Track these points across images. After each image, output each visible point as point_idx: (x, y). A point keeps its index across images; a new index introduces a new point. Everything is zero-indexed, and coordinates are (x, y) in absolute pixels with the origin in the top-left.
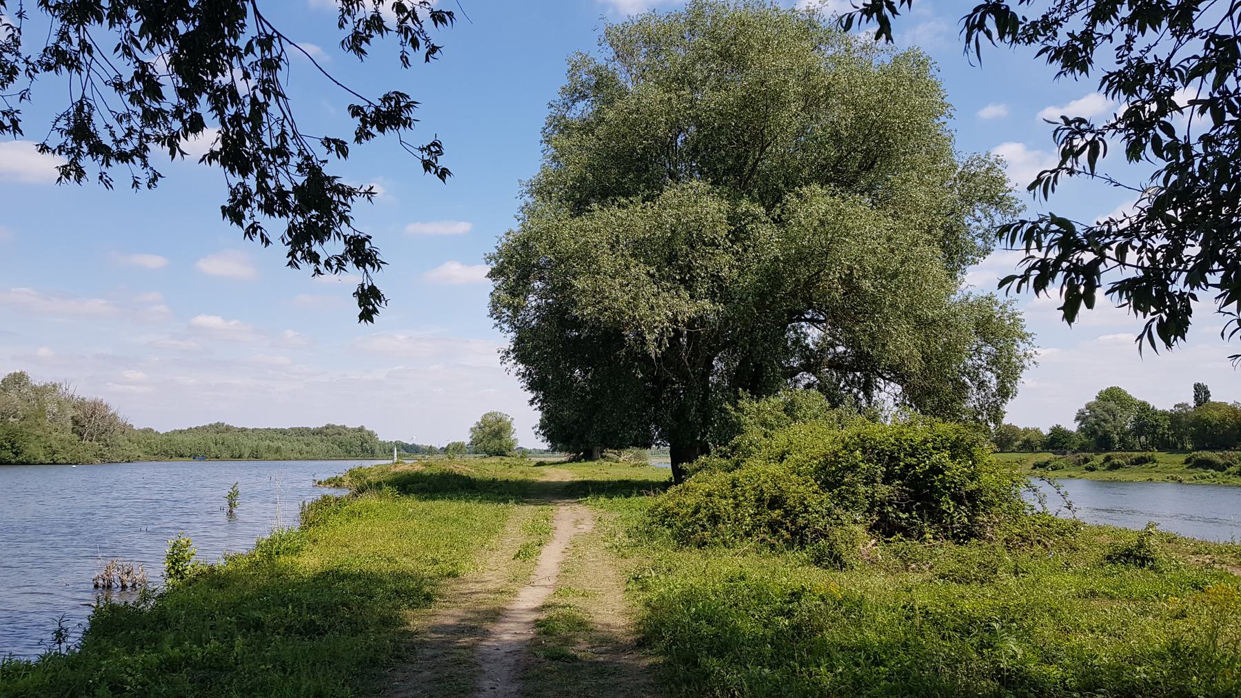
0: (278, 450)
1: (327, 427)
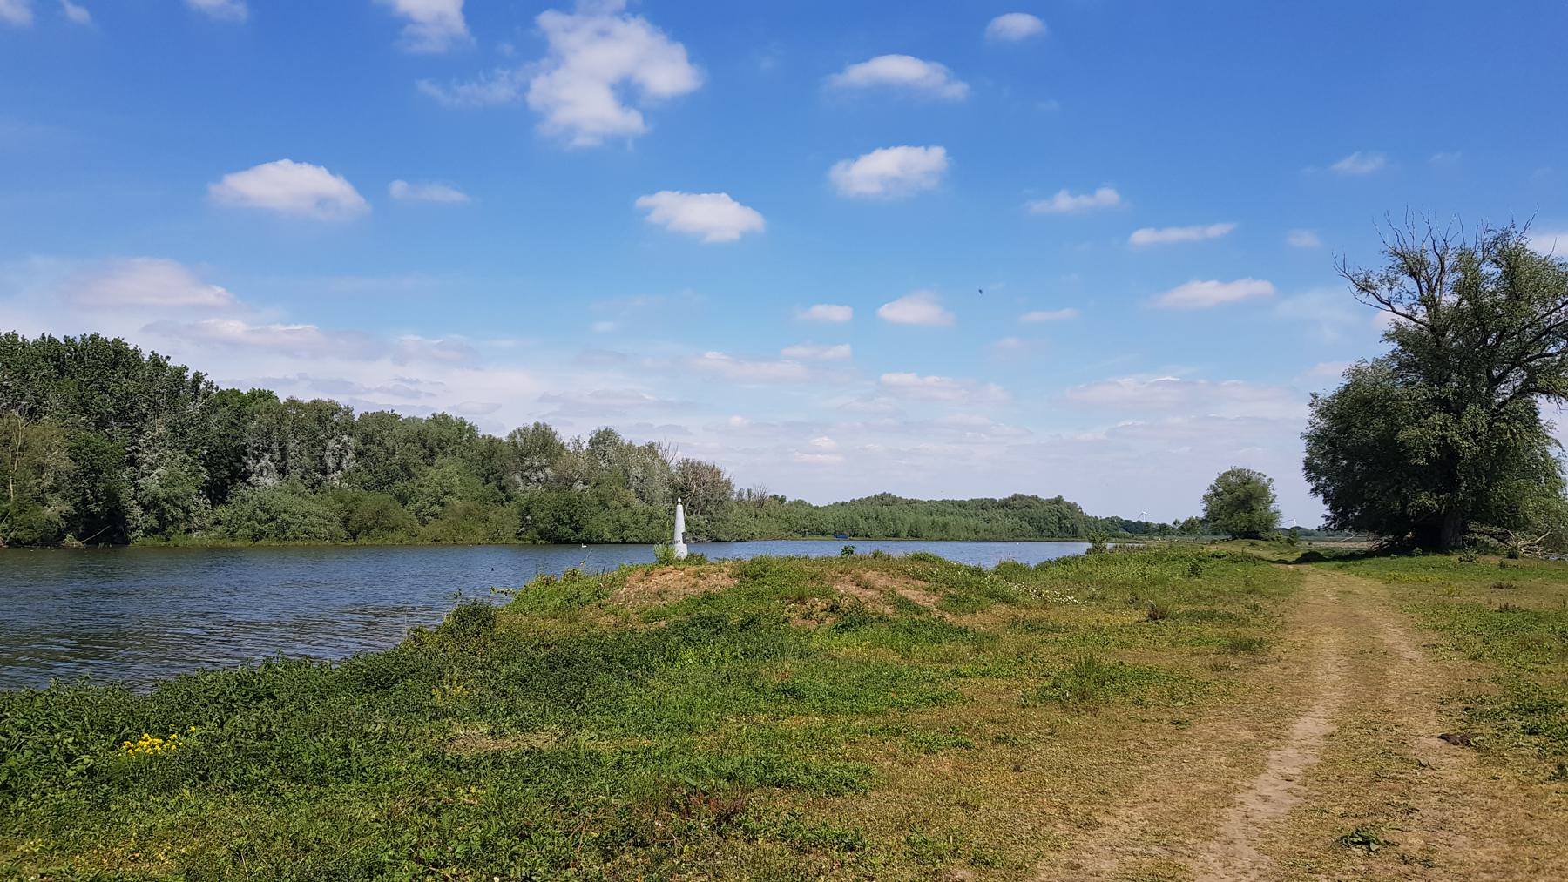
0: (945, 527)
1: (1014, 498)
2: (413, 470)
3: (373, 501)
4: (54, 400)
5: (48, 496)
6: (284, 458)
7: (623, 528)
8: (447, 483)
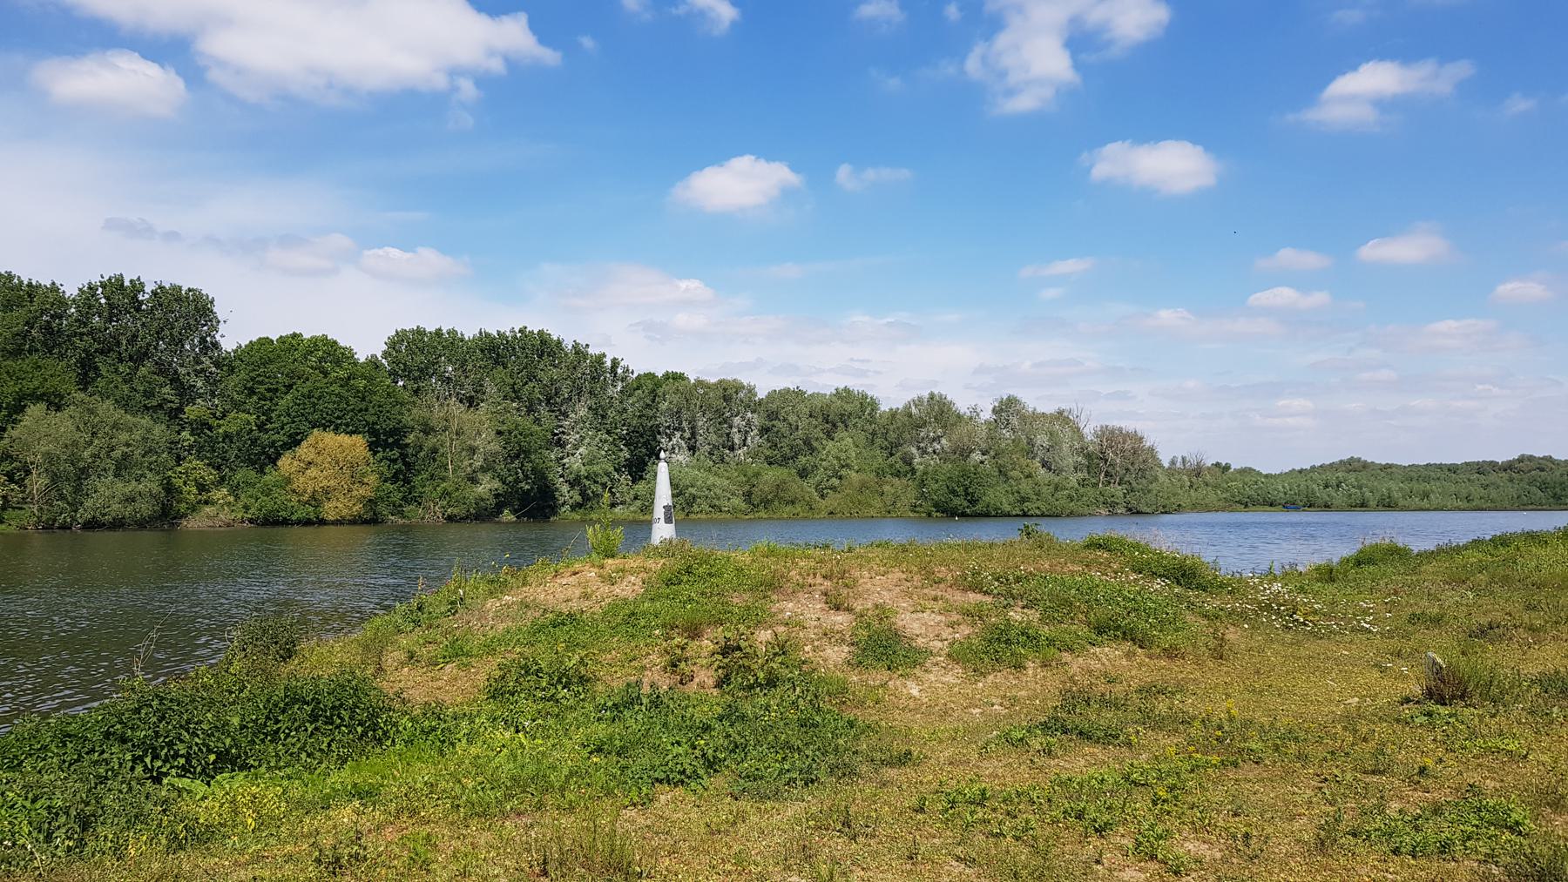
1: (1521, 459)
2: (815, 444)
3: (772, 475)
4: (490, 388)
5: (480, 476)
6: (693, 434)
7: (1023, 500)
8: (843, 456)
